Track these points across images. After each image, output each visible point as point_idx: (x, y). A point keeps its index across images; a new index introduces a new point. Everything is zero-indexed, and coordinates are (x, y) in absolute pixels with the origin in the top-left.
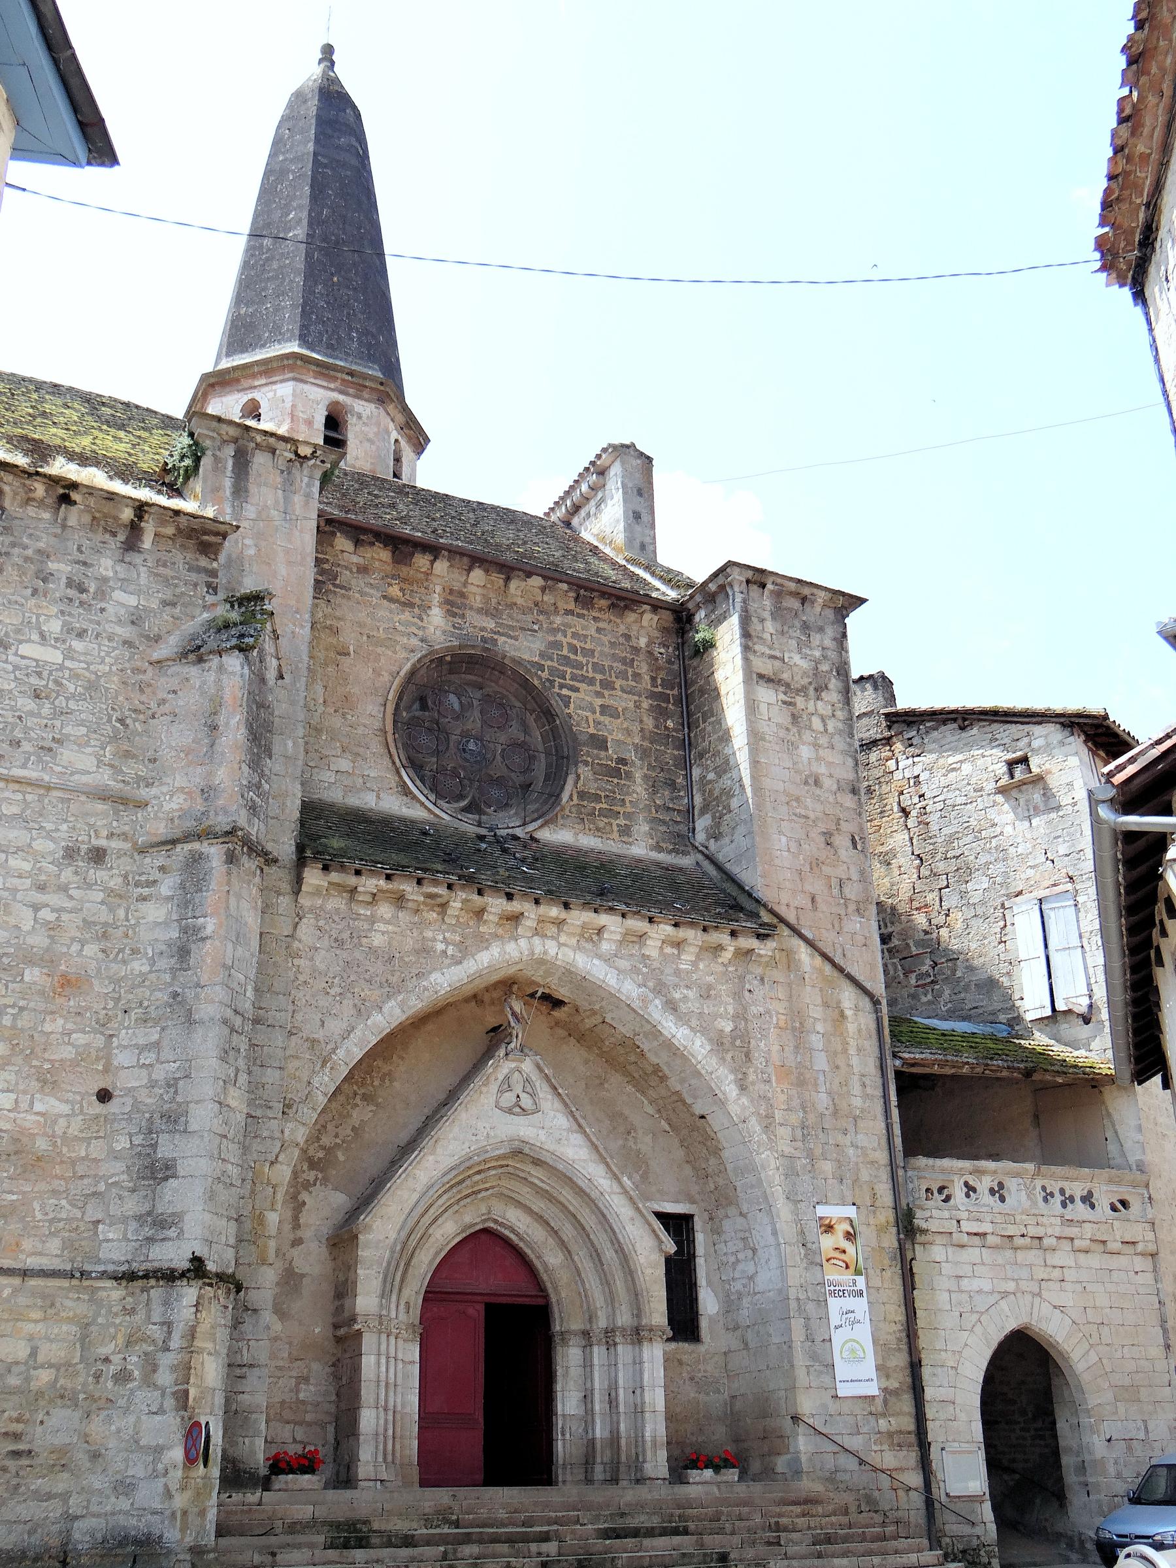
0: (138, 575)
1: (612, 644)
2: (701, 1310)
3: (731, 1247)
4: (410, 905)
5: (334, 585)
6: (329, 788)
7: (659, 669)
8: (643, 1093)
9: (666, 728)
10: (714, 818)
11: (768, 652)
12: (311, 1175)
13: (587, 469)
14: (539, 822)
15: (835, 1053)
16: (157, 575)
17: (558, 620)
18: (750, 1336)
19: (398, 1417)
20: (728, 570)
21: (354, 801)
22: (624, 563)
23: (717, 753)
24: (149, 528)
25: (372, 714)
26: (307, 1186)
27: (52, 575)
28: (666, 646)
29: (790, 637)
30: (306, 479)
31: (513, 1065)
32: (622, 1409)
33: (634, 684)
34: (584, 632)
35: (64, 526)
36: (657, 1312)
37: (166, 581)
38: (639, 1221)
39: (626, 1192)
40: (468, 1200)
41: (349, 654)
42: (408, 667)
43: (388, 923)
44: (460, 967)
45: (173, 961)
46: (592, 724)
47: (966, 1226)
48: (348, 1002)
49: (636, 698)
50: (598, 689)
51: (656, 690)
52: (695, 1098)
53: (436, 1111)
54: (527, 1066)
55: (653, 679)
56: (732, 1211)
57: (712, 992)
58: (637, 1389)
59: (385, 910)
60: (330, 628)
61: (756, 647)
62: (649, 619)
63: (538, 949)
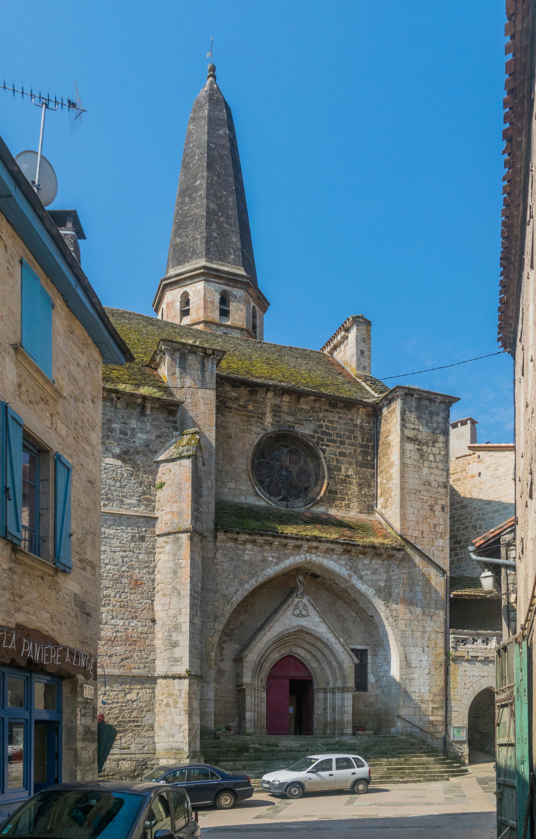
0: (146, 426)
1: (345, 424)
2: (368, 681)
3: (381, 661)
4: (258, 544)
5: (225, 407)
6: (226, 495)
7: (365, 433)
8: (350, 607)
9: (367, 460)
10: (385, 500)
11: (412, 426)
12: (226, 638)
13: (340, 328)
14: (311, 504)
15: (426, 593)
16: (153, 425)
17: (321, 415)
18: (385, 690)
19: (259, 714)
20: (397, 389)
21: (236, 500)
22: (355, 377)
23: (387, 472)
24: (148, 405)
25: (243, 464)
26: (224, 642)
27: (113, 429)
28: (369, 423)
29: (423, 419)
30: (210, 365)
31: (299, 600)
32: (337, 712)
33: (354, 441)
34: (333, 419)
35: (116, 408)
36: (351, 683)
37: (157, 427)
38: (345, 653)
39: (341, 643)
40: (283, 646)
41: (232, 438)
42: (256, 441)
43: (250, 551)
44: (278, 566)
45: (172, 575)
46: (335, 461)
47: (471, 654)
48: (236, 581)
49: (355, 447)
50: (338, 444)
51: (363, 443)
52: (369, 610)
53: (271, 616)
54: (305, 600)
55: (363, 438)
56: (382, 649)
57: (378, 572)
58: (343, 706)
59: (249, 546)
60: (224, 427)
61: (407, 425)
62: (362, 411)
63: (308, 558)
